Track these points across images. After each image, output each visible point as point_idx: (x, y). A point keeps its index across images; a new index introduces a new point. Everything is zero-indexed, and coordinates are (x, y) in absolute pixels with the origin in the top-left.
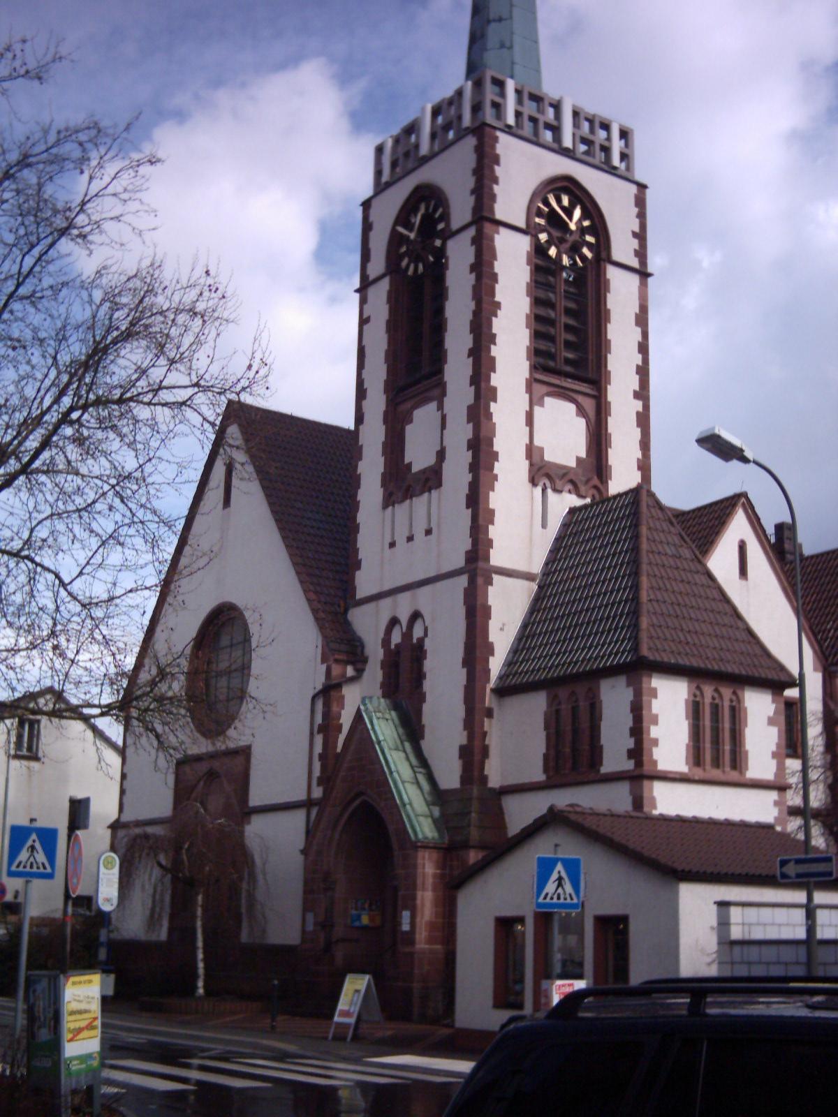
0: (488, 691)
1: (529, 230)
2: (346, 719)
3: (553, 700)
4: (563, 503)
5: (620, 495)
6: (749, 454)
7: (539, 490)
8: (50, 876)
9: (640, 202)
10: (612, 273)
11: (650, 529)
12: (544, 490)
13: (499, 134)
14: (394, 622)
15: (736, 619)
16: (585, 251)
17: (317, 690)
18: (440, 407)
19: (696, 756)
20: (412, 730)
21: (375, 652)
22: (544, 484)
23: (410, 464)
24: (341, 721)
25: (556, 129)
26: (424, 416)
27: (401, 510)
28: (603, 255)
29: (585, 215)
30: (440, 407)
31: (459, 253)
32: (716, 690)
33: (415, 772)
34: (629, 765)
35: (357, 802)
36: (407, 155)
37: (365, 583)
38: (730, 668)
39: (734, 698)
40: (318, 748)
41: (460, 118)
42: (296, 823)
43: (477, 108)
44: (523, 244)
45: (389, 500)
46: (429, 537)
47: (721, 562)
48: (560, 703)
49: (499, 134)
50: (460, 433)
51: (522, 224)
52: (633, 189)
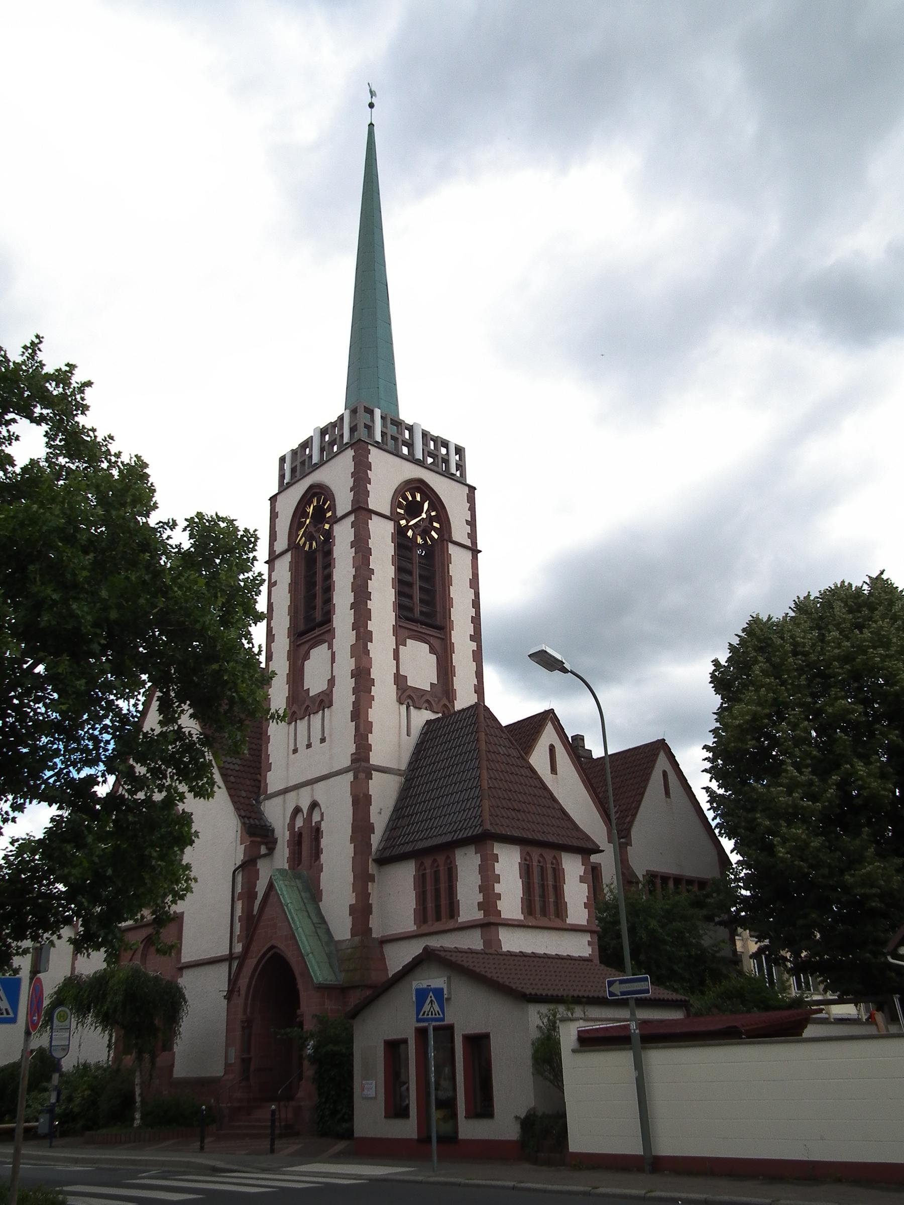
0: (370, 860)
1: (393, 517)
2: (261, 887)
3: (420, 867)
4: (422, 717)
5: (463, 710)
6: (567, 666)
7: (405, 706)
8: (13, 1021)
9: (471, 499)
10: (452, 549)
11: (486, 734)
12: (408, 708)
13: (370, 447)
14: (297, 810)
15: (553, 802)
16: (433, 533)
17: (237, 865)
18: (330, 647)
19: (528, 906)
20: (313, 893)
21: (283, 835)
22: (408, 703)
24: (256, 890)
25: (410, 445)
26: (319, 654)
28: (446, 537)
29: (432, 507)
30: (330, 647)
31: (343, 534)
32: (541, 855)
33: (315, 927)
34: (479, 915)
36: (303, 463)
37: (274, 780)
38: (551, 839)
39: (554, 861)
40: (239, 912)
41: (342, 436)
42: (219, 978)
43: (353, 430)
44: (390, 527)
47: (539, 759)
48: (425, 869)
49: (370, 447)
50: (346, 665)
51: (388, 513)
52: (466, 490)
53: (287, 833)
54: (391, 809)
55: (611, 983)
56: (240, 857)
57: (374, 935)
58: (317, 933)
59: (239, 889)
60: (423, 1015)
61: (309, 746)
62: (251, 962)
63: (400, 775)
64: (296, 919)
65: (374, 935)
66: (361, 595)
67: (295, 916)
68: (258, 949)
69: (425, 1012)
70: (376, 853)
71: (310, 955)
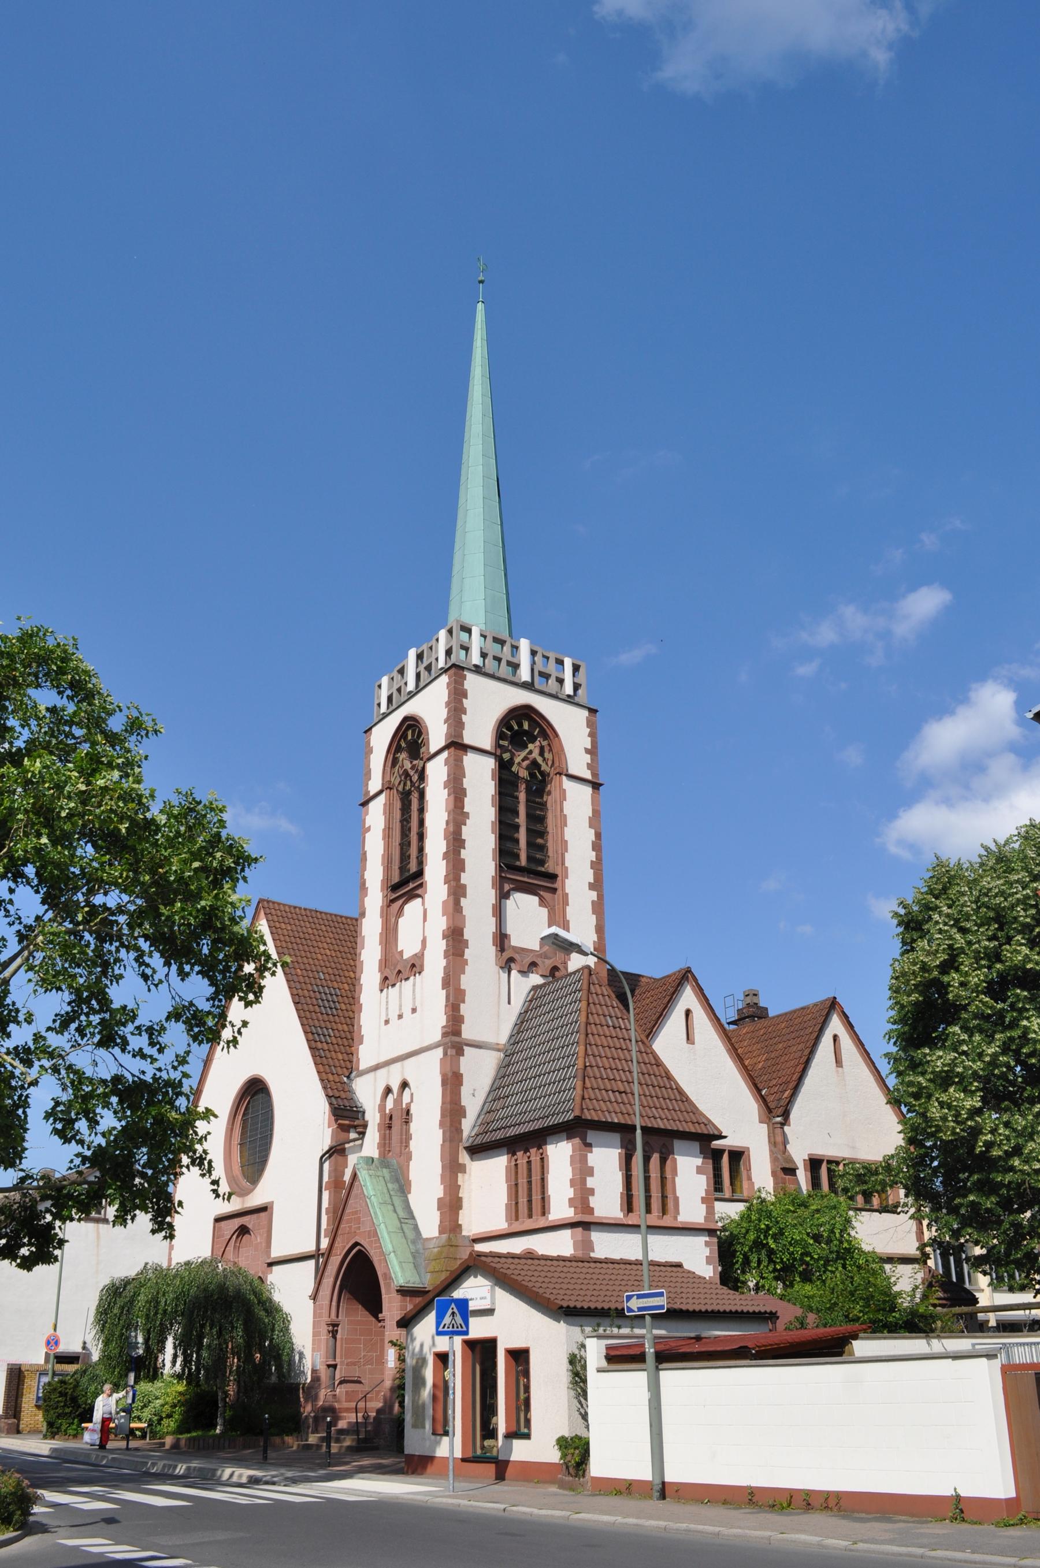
14: (388, 1090)
20: (402, 1186)
23: (402, 951)
26: (413, 907)
27: (393, 992)
31: (437, 771)
35: (354, 1251)
36: (399, 690)
37: (366, 1055)
44: (490, 763)
45: (386, 982)
46: (414, 1015)
50: (439, 923)
53: (378, 1116)
54: (487, 1089)
55: (629, 1298)
56: (326, 1143)
57: (464, 1233)
58: (402, 1230)
59: (326, 1178)
60: (444, 1327)
61: (400, 1017)
62: (335, 1261)
63: (499, 1050)
64: (379, 1213)
65: (464, 1233)
66: (456, 842)
67: (378, 1210)
68: (342, 1246)
69: (445, 1325)
70: (468, 1140)
71: (392, 1254)
